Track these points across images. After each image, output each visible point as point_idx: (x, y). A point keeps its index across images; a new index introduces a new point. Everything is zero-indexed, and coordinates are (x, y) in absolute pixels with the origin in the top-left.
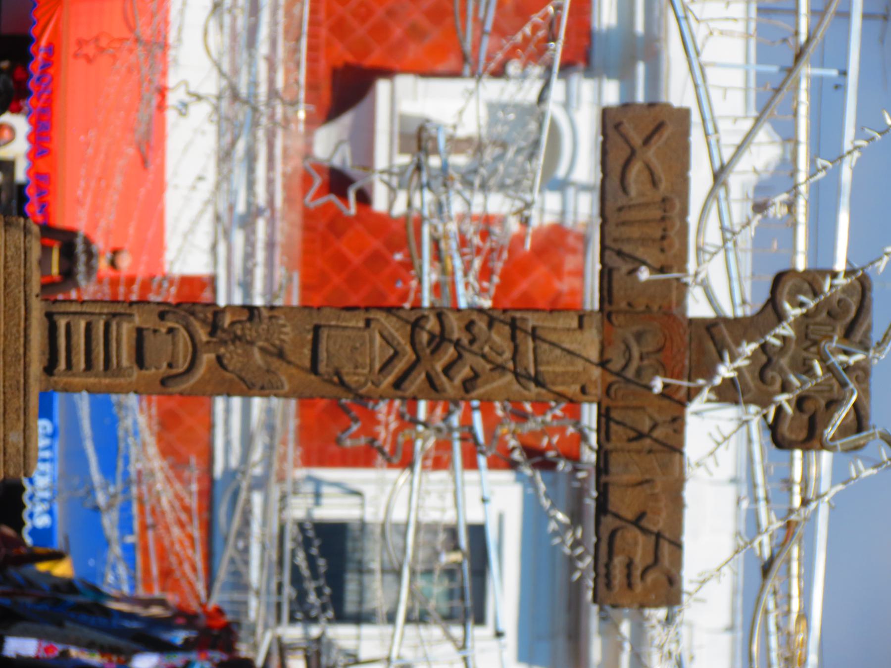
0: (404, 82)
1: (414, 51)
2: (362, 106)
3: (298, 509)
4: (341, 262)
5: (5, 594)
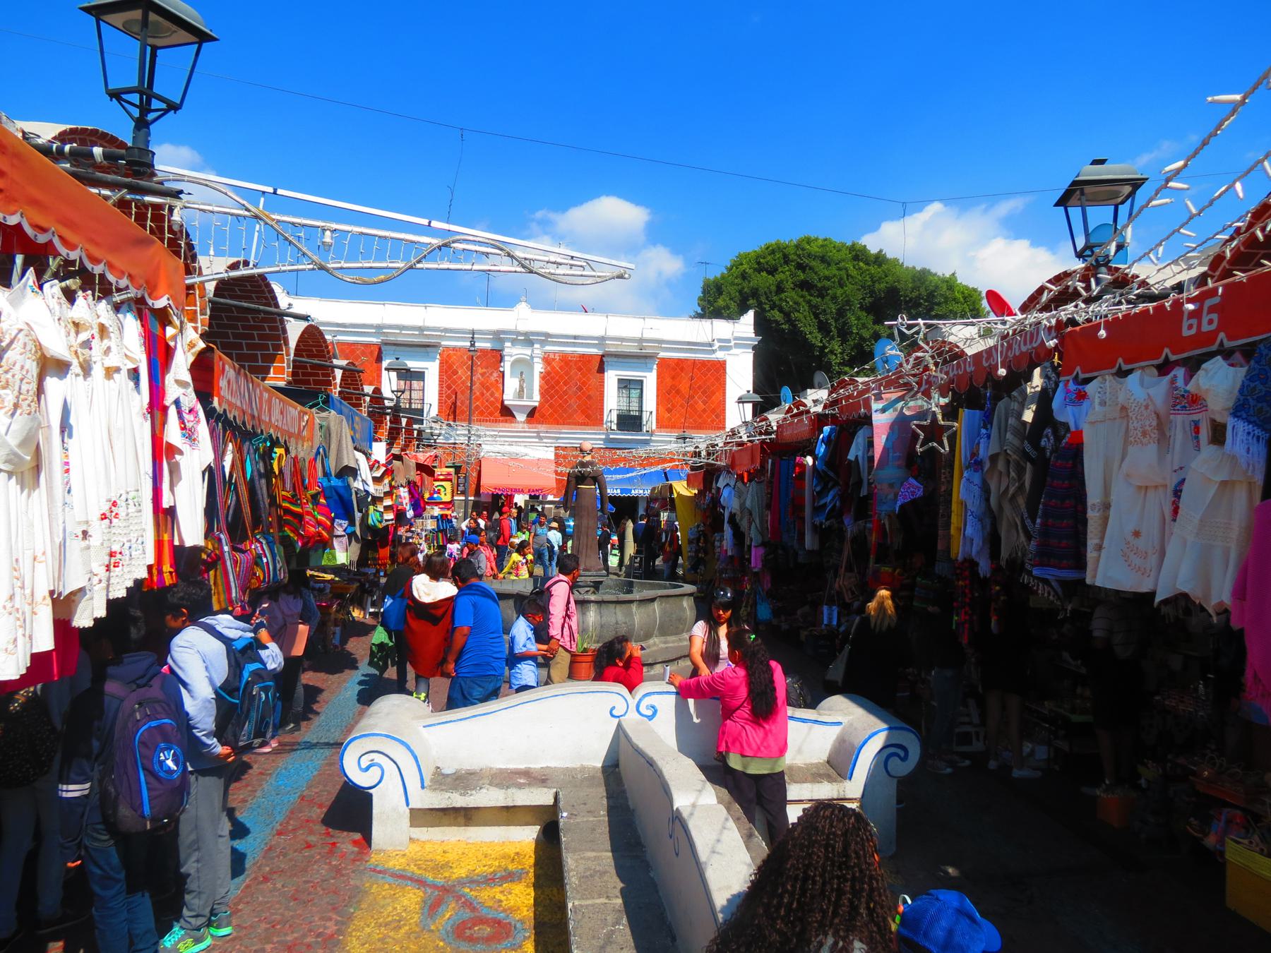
0: (505, 397)
1: (497, 395)
2: (511, 408)
3: (614, 427)
4: (551, 415)
5: (760, 951)
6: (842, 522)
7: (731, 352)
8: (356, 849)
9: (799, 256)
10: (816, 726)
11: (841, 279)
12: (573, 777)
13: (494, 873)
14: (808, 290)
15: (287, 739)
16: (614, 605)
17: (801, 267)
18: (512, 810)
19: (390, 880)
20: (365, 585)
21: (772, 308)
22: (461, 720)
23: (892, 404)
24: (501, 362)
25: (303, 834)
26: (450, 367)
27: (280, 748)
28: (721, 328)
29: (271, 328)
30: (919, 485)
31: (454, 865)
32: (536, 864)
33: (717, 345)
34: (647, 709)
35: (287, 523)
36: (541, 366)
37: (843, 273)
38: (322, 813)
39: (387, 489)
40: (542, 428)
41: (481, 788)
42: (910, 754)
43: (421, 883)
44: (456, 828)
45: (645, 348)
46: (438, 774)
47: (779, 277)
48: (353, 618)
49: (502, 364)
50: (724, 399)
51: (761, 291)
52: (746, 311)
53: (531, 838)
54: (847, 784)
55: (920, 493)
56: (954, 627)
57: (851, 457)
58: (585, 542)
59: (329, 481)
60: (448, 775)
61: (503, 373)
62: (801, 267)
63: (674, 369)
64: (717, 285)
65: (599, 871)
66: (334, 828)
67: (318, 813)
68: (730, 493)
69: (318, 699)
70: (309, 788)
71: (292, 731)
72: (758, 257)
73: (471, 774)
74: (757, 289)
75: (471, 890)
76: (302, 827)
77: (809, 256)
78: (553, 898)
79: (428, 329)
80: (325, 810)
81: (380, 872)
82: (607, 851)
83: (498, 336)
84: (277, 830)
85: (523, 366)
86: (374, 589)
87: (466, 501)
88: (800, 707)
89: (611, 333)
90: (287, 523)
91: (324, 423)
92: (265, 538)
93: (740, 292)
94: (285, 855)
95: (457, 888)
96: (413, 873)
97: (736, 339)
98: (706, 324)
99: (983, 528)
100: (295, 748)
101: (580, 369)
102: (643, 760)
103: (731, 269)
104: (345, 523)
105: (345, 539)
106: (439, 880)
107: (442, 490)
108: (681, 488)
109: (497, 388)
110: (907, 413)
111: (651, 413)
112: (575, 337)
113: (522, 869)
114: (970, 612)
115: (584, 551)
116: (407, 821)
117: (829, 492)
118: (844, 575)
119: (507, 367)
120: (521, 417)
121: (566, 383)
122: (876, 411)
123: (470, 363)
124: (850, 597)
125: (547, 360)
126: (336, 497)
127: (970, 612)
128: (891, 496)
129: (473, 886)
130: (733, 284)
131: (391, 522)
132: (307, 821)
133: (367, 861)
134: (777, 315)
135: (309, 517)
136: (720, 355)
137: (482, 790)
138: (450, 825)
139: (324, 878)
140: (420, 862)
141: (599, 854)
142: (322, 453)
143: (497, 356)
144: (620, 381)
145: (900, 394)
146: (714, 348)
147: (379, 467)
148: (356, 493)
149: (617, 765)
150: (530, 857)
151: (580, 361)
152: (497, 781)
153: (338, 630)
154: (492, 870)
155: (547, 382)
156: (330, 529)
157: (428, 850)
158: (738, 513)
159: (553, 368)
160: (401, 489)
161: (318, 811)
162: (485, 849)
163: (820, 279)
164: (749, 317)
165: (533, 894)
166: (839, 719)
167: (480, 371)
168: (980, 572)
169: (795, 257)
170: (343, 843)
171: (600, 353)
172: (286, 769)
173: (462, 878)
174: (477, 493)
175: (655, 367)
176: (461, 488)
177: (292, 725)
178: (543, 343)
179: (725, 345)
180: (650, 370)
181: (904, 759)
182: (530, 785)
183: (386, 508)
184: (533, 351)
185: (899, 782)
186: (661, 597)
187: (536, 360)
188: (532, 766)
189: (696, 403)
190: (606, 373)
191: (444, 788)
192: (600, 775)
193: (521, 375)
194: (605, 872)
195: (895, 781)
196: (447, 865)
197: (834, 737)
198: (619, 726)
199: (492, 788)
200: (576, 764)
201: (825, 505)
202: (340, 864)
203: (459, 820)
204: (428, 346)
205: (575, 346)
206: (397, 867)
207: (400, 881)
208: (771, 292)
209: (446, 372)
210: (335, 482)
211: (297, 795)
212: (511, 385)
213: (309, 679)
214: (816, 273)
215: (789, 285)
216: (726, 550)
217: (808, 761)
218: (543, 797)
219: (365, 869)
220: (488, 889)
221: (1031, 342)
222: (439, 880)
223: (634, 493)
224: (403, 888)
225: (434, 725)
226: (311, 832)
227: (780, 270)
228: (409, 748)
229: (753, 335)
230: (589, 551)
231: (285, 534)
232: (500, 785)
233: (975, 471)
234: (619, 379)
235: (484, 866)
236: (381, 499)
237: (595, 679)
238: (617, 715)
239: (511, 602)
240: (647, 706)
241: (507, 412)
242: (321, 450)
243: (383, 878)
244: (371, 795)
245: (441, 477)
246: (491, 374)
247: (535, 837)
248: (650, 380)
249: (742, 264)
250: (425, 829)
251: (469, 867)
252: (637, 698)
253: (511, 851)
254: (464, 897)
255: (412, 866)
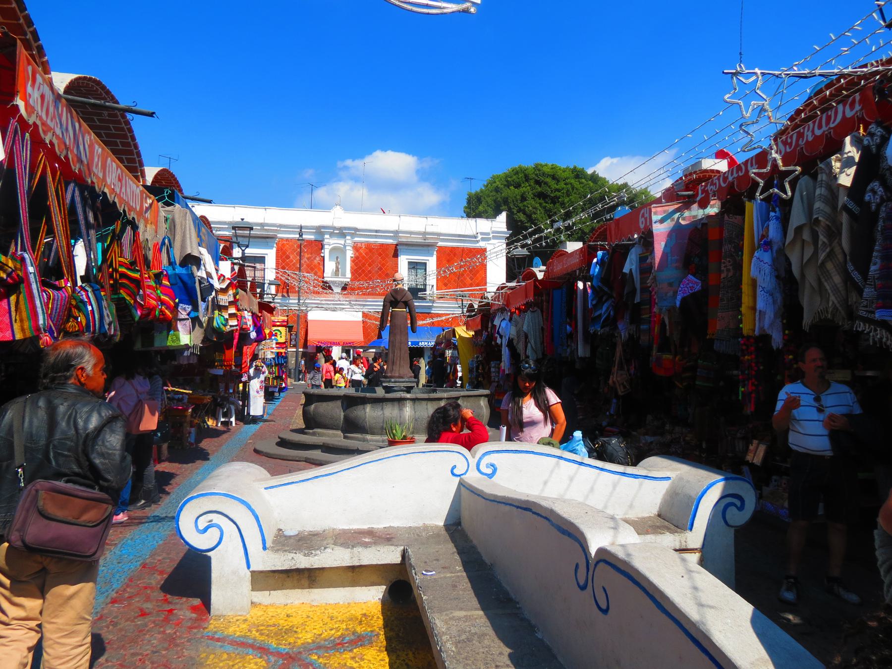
6: (616, 328)
7: (490, 242)
8: (194, 615)
9: (536, 175)
10: (647, 482)
11: (568, 191)
12: (418, 535)
13: (343, 636)
14: (544, 199)
15: (139, 513)
16: (426, 402)
17: (538, 182)
18: (357, 570)
19: (230, 648)
20: (217, 399)
21: (518, 212)
22: (303, 481)
23: (669, 216)
24: (322, 249)
25: (138, 601)
26: (284, 253)
27: (129, 521)
28: (483, 225)
29: (123, 144)
30: (698, 281)
31: (299, 630)
32: (386, 626)
33: (480, 237)
34: (487, 467)
35: (123, 286)
36: (352, 252)
37: (569, 186)
38: (162, 579)
39: (232, 299)
40: (353, 298)
41: (325, 548)
42: (746, 503)
43: (263, 650)
44: (300, 590)
45: (427, 239)
46: (281, 536)
47: (522, 190)
48: (208, 425)
49: (323, 251)
50: (486, 276)
51: (510, 200)
52: (501, 213)
53: (377, 598)
54: (689, 534)
55: (698, 288)
56: (740, 398)
57: (626, 270)
58: (399, 355)
59: (174, 269)
60: (290, 537)
61: (323, 257)
62: (538, 182)
63: (449, 255)
64: (478, 197)
65: (476, 633)
66: (172, 594)
67: (157, 580)
68: (507, 325)
69: (170, 482)
70: (152, 556)
71: (143, 507)
72: (507, 176)
73: (314, 535)
74: (507, 198)
75: (319, 658)
76: (138, 594)
77: (543, 175)
78: (410, 663)
79: (268, 225)
80: (165, 576)
81: (218, 640)
82: (476, 609)
83: (320, 230)
84: (112, 598)
85: (338, 253)
86: (225, 403)
87: (297, 352)
88: (628, 465)
89: (402, 228)
90: (123, 286)
91: (169, 216)
92: (91, 286)
93: (495, 201)
94: (115, 624)
95: (304, 656)
96: (255, 639)
97: (493, 232)
98: (472, 221)
99: (774, 302)
100: (143, 521)
101: (380, 255)
102: (508, 508)
103: (487, 186)
104: (189, 308)
105: (189, 323)
106: (284, 647)
107: (279, 333)
108: (462, 332)
109: (319, 269)
110: (683, 223)
111: (433, 286)
112: (377, 231)
113: (372, 631)
114: (756, 383)
115: (398, 362)
116: (247, 584)
117: (604, 304)
118: (617, 373)
119: (326, 253)
120: (337, 290)
121: (370, 265)
122: (655, 223)
123: (299, 250)
124: (623, 390)
125: (356, 248)
126: (180, 284)
127: (756, 383)
128: (671, 293)
129: (320, 652)
130: (488, 196)
131: (235, 328)
132: (146, 588)
133: (204, 628)
134: (522, 217)
135: (150, 291)
136: (482, 244)
137: (326, 551)
138: (294, 588)
139: (155, 650)
140: (262, 628)
141: (469, 613)
142: (167, 244)
143: (319, 245)
144: (410, 263)
145: (676, 206)
146: (477, 239)
147: (224, 280)
148: (200, 283)
149: (458, 523)
150: (378, 618)
151: (380, 249)
152: (342, 541)
153: (193, 430)
154: (339, 633)
155: (356, 264)
156: (175, 309)
157: (271, 614)
158: (516, 338)
159: (360, 254)
160: (246, 312)
161: (159, 577)
162: (330, 611)
163: (552, 191)
164: (503, 217)
165: (387, 660)
166: (668, 474)
167: (306, 256)
168: (773, 345)
169: (534, 176)
170: (181, 609)
171: (395, 242)
172: (132, 539)
173: (308, 643)
174: (305, 346)
175: (435, 253)
176: (293, 343)
177: (143, 502)
178: (353, 236)
179: (486, 237)
180: (432, 255)
181: (741, 508)
182: (375, 543)
183: (231, 315)
184: (345, 241)
185: (735, 530)
186: (462, 396)
187: (348, 248)
188: (375, 526)
189: (465, 279)
190: (399, 258)
191: (287, 548)
192: (443, 532)
193: (337, 259)
194: (484, 635)
195: (732, 530)
196: (291, 631)
197: (664, 491)
198: (462, 484)
199: (336, 548)
200: (419, 523)
201: (600, 316)
202: (175, 633)
203: (303, 582)
204: (268, 238)
205: (376, 238)
206: (238, 634)
207: (240, 649)
208: (517, 201)
209: (281, 257)
210: (179, 270)
211: (139, 563)
212: (330, 267)
213: (165, 467)
214: (549, 187)
215: (530, 196)
216: (504, 370)
217: (640, 516)
218: (390, 556)
219: (202, 637)
220: (338, 654)
221: (828, 123)
222: (284, 647)
223: (422, 344)
224: (243, 657)
225: (276, 486)
226: (148, 599)
227: (523, 185)
228: (249, 507)
229: (506, 230)
230: (402, 362)
231: (121, 296)
232: (345, 545)
233: (764, 251)
234: (409, 262)
235: (331, 630)
236: (226, 308)
237: (427, 441)
238: (458, 474)
239: (339, 403)
240: (487, 464)
241: (327, 286)
242: (166, 241)
243: (221, 647)
244: (209, 558)
245: (278, 324)
246: (315, 259)
247: (381, 597)
248: (432, 263)
249: (495, 182)
250: (267, 593)
251: (315, 631)
252: (478, 456)
253: (358, 613)
254: (312, 665)
255: (254, 632)
